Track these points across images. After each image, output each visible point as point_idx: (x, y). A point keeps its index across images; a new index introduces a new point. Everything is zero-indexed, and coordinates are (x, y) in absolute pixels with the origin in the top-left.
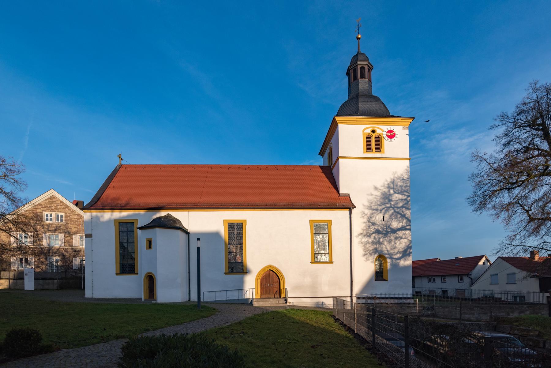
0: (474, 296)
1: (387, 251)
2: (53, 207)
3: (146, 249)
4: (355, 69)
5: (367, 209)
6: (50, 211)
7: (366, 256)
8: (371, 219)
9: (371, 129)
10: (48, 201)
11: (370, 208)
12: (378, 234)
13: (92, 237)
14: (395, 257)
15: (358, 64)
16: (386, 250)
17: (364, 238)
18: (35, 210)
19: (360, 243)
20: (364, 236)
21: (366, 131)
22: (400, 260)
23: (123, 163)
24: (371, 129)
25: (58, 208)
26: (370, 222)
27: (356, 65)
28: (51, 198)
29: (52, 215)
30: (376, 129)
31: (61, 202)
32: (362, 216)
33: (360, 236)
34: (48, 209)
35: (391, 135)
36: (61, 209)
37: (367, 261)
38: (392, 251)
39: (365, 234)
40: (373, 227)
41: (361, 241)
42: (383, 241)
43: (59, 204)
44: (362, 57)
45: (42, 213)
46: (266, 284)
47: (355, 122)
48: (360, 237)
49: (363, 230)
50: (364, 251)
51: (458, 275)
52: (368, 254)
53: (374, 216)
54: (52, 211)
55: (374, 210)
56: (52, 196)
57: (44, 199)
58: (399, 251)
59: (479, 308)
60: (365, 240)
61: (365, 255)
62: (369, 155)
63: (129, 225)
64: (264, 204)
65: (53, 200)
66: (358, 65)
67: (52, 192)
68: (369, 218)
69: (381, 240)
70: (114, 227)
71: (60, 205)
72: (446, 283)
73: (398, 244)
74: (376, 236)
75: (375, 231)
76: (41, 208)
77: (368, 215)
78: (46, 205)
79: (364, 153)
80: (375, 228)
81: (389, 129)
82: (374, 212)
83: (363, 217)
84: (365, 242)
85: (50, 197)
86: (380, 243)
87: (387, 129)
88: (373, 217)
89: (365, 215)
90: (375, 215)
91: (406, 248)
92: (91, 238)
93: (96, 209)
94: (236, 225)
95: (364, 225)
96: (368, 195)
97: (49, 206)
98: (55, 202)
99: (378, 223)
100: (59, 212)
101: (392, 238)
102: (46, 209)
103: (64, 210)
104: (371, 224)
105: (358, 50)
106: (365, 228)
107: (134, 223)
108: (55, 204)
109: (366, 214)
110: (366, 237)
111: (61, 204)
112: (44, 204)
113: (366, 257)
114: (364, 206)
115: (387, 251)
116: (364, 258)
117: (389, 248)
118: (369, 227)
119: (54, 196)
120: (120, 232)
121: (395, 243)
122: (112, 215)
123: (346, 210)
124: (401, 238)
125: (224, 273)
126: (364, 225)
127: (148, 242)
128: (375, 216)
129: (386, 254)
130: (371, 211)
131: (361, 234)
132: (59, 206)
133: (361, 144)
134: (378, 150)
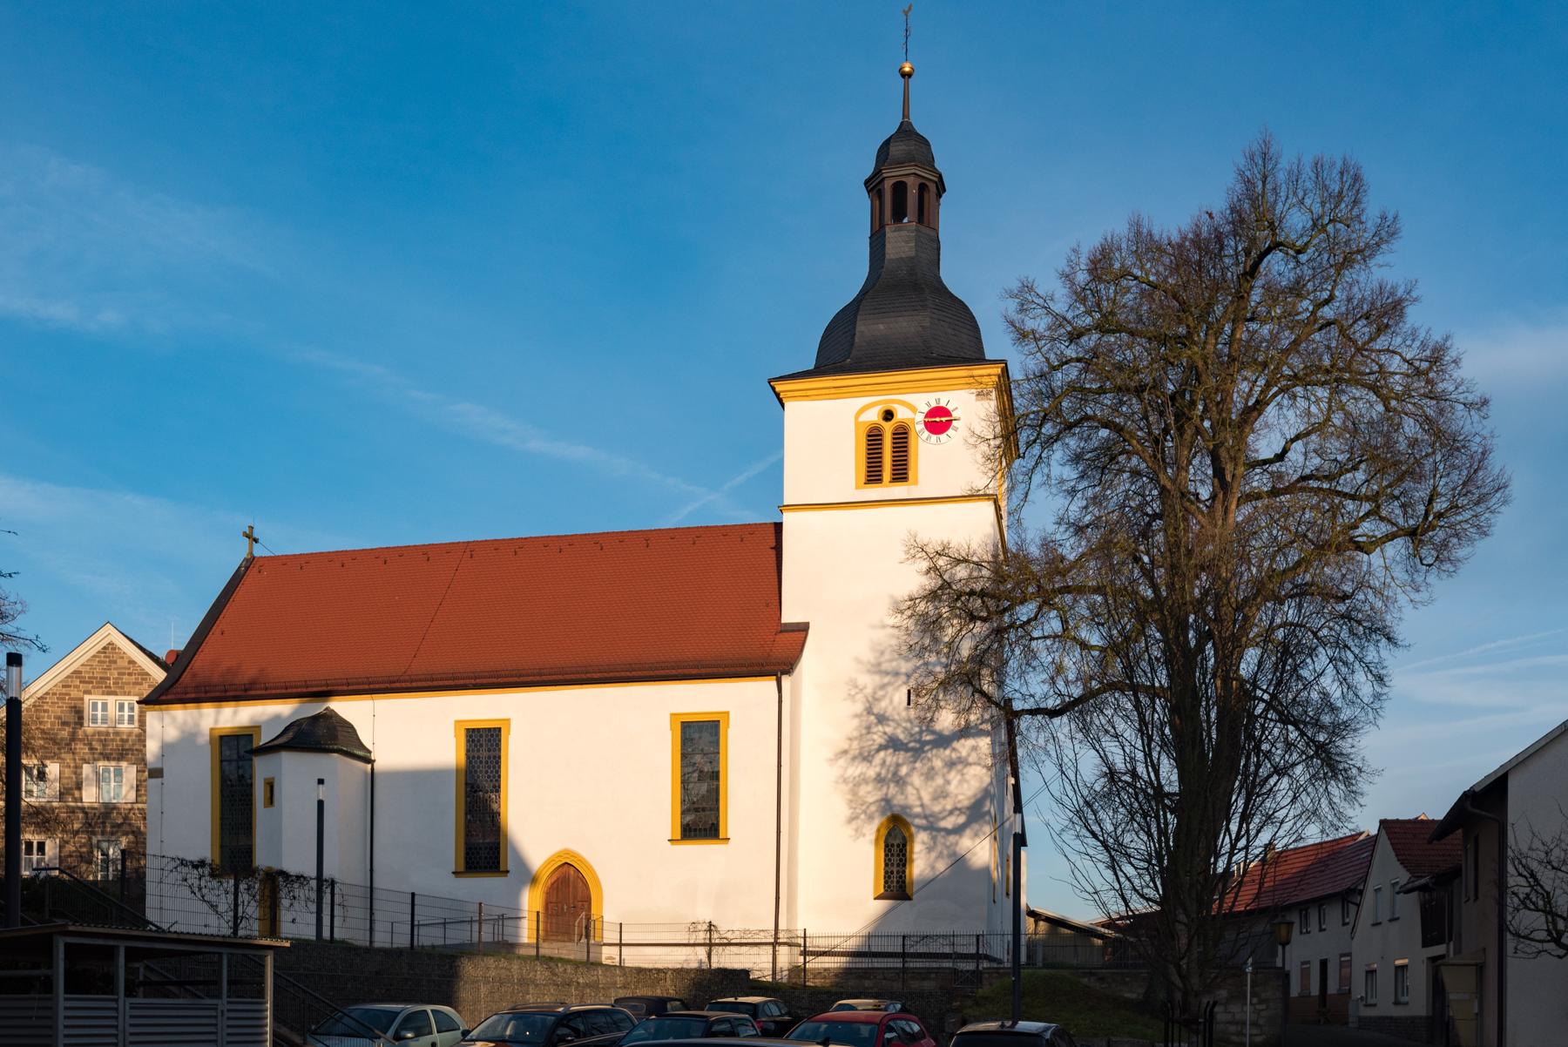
1: (922, 806)
2: (109, 679)
3: (265, 807)
4: (880, 190)
5: (869, 671)
6: (103, 694)
7: (854, 822)
8: (876, 703)
9: (881, 406)
10: (99, 662)
11: (877, 669)
12: (895, 750)
13: (162, 777)
14: (943, 824)
15: (885, 175)
16: (918, 803)
17: (853, 765)
18: (64, 690)
19: (840, 781)
20: (854, 758)
21: (863, 418)
22: (961, 836)
23: (259, 551)
24: (881, 406)
25: (122, 683)
26: (873, 714)
27: (881, 178)
28: (105, 653)
29: (106, 703)
30: (894, 405)
31: (132, 662)
32: (849, 695)
33: (840, 758)
34: (98, 688)
35: (939, 421)
36: (129, 683)
37: (858, 838)
38: (937, 808)
39: (857, 752)
40: (880, 728)
41: (842, 776)
42: (908, 775)
43: (125, 668)
44: (900, 148)
45: (82, 699)
46: (560, 905)
47: (833, 391)
48: (842, 762)
49: (850, 739)
50: (851, 808)
52: (863, 816)
53: (887, 693)
54: (109, 693)
55: (887, 673)
56: (109, 644)
57: (88, 658)
58: (959, 806)
59: (1092, 979)
60: (857, 770)
61: (852, 819)
62: (874, 493)
63: (242, 743)
64: (507, 672)
65: (109, 657)
66: (884, 178)
67: (107, 633)
68: (870, 699)
69: (904, 770)
70: (453, 741)
71: (127, 671)
73: (954, 783)
74: (889, 759)
75: (888, 741)
76: (81, 685)
77: (869, 691)
78: (93, 673)
79: (857, 487)
80: (885, 733)
81: (934, 405)
82: (886, 679)
83: (852, 697)
84: (855, 778)
85: (105, 648)
86: (900, 782)
87: (928, 404)
88: (884, 696)
89: (857, 690)
90: (890, 689)
91: (979, 796)
92: (160, 780)
93: (183, 701)
94: (487, 736)
95: (856, 722)
96: (873, 627)
97: (101, 678)
98: (115, 662)
99: (896, 717)
100: (125, 694)
101: (938, 763)
102: (93, 687)
103: (138, 687)
104: (875, 721)
105: (904, 116)
106: (855, 734)
107: (251, 735)
108: (115, 669)
109: (861, 687)
110: (860, 762)
111: (129, 668)
112: (89, 672)
113: (854, 824)
114: (859, 661)
115: (922, 806)
116: (849, 831)
117: (926, 798)
118: (868, 728)
119: (113, 644)
120: (221, 761)
121: (948, 782)
122: (235, 713)
123: (770, 680)
124: (968, 764)
125: (453, 873)
126: (856, 722)
127: (268, 788)
128: (888, 696)
129: (917, 816)
130: (877, 679)
131: (845, 752)
132: (124, 674)
133: (848, 457)
134: (901, 475)
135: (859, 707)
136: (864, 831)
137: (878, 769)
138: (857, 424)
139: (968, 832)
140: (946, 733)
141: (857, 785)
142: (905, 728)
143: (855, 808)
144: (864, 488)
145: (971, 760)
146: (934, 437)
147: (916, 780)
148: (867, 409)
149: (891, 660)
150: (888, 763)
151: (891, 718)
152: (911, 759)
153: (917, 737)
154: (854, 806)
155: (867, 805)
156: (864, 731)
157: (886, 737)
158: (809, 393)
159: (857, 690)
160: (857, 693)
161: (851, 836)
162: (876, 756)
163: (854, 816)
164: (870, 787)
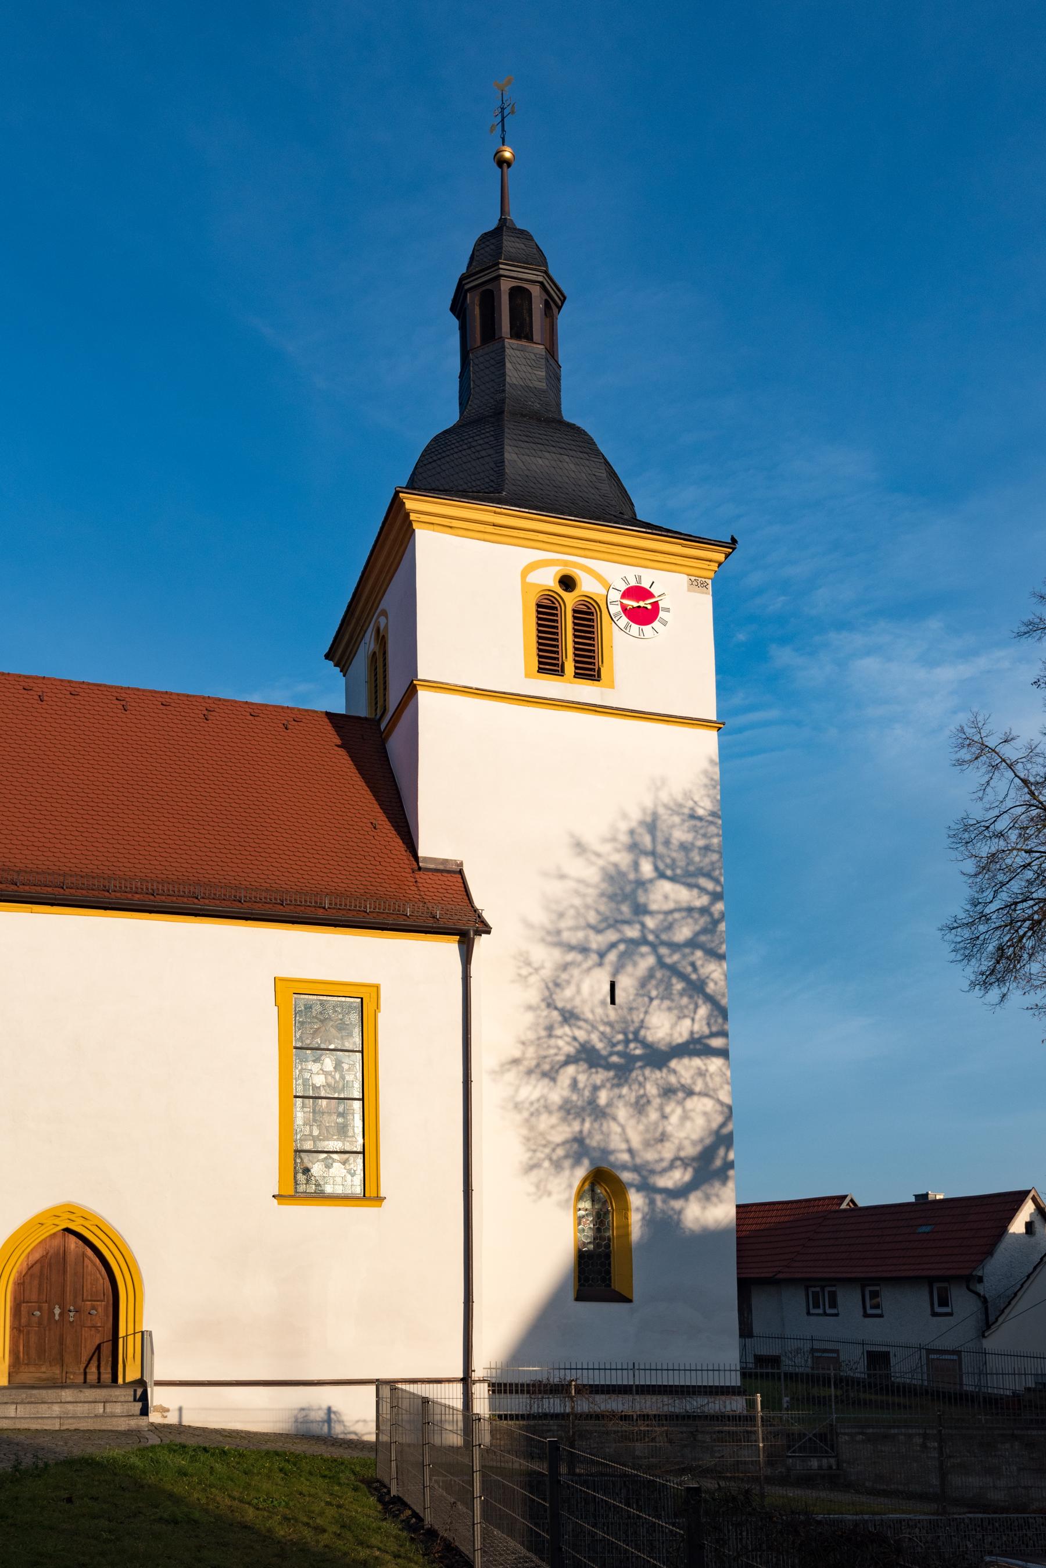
0: (1007, 1385)
1: (630, 1151)
5: (543, 940)
7: (535, 1172)
8: (558, 990)
12: (591, 1066)
17: (528, 1083)
19: (511, 1106)
20: (529, 1072)
22: (687, 1200)
26: (556, 1008)
32: (519, 975)
33: (509, 1070)
37: (540, 1197)
38: (650, 1156)
39: (534, 1063)
40: (567, 1029)
42: (610, 1104)
47: (490, 529)
50: (529, 1150)
51: (931, 1281)
52: (546, 1164)
55: (571, 948)
58: (682, 1154)
60: (533, 1090)
61: (532, 1167)
68: (551, 985)
72: (881, 1316)
73: (674, 1119)
74: (582, 1078)
75: (578, 1052)
77: (547, 973)
80: (575, 1039)
81: (633, 583)
82: (571, 957)
84: (532, 1104)
86: (600, 1113)
87: (625, 579)
88: (568, 982)
90: (576, 972)
91: (708, 1141)
95: (529, 1017)
96: (545, 874)
101: (651, 1090)
104: (560, 1018)
106: (531, 1035)
109: (536, 965)
110: (538, 1080)
114: (529, 925)
115: (630, 1151)
116: (527, 1184)
117: (636, 1142)
121: (664, 1117)
124: (690, 1093)
126: (529, 1017)
131: (516, 1062)
135: (533, 995)
136: (550, 1187)
137: (566, 1093)
138: (526, 586)
139: (693, 1197)
140: (663, 1047)
141: (534, 1114)
142: (603, 1033)
143: (534, 1151)
144: (538, 678)
145: (698, 1088)
146: (647, 628)
147: (622, 1113)
148: (538, 568)
149: (575, 929)
150: (581, 1085)
151: (582, 1016)
152: (615, 1081)
153: (620, 1048)
154: (533, 1147)
155: (552, 1146)
156: (543, 1033)
157: (576, 1044)
158: (454, 523)
159: (531, 970)
160: (531, 974)
161: (529, 1194)
162: (562, 1071)
163: (532, 1162)
164: (554, 1120)
